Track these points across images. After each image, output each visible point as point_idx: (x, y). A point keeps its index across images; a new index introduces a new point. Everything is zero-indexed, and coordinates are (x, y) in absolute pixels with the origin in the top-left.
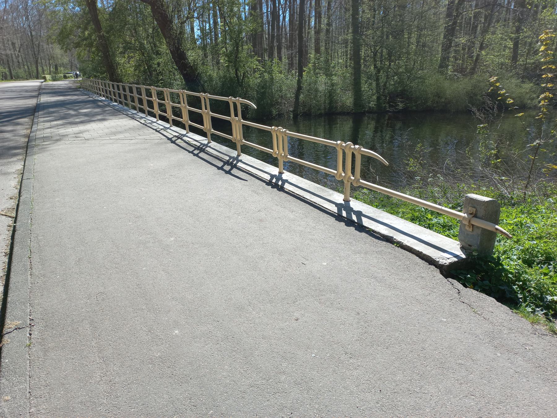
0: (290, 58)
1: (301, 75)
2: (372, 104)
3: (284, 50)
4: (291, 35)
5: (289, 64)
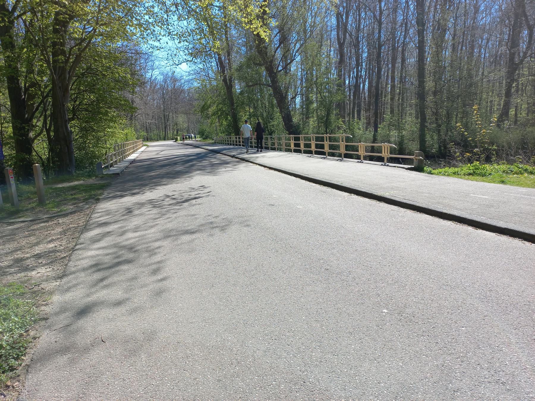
0: (368, 118)
1: (376, 130)
2: (434, 151)
3: (362, 112)
4: (369, 102)
5: (367, 123)
